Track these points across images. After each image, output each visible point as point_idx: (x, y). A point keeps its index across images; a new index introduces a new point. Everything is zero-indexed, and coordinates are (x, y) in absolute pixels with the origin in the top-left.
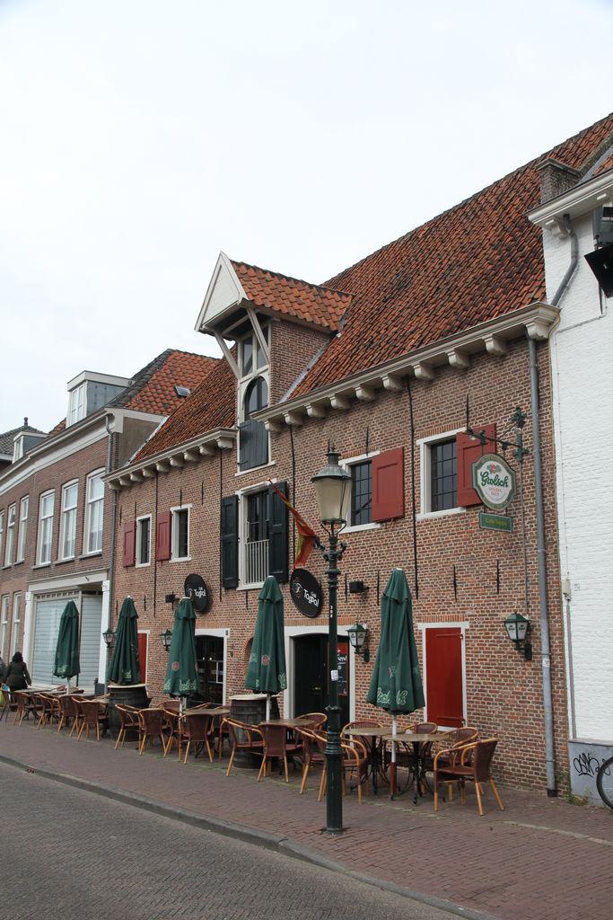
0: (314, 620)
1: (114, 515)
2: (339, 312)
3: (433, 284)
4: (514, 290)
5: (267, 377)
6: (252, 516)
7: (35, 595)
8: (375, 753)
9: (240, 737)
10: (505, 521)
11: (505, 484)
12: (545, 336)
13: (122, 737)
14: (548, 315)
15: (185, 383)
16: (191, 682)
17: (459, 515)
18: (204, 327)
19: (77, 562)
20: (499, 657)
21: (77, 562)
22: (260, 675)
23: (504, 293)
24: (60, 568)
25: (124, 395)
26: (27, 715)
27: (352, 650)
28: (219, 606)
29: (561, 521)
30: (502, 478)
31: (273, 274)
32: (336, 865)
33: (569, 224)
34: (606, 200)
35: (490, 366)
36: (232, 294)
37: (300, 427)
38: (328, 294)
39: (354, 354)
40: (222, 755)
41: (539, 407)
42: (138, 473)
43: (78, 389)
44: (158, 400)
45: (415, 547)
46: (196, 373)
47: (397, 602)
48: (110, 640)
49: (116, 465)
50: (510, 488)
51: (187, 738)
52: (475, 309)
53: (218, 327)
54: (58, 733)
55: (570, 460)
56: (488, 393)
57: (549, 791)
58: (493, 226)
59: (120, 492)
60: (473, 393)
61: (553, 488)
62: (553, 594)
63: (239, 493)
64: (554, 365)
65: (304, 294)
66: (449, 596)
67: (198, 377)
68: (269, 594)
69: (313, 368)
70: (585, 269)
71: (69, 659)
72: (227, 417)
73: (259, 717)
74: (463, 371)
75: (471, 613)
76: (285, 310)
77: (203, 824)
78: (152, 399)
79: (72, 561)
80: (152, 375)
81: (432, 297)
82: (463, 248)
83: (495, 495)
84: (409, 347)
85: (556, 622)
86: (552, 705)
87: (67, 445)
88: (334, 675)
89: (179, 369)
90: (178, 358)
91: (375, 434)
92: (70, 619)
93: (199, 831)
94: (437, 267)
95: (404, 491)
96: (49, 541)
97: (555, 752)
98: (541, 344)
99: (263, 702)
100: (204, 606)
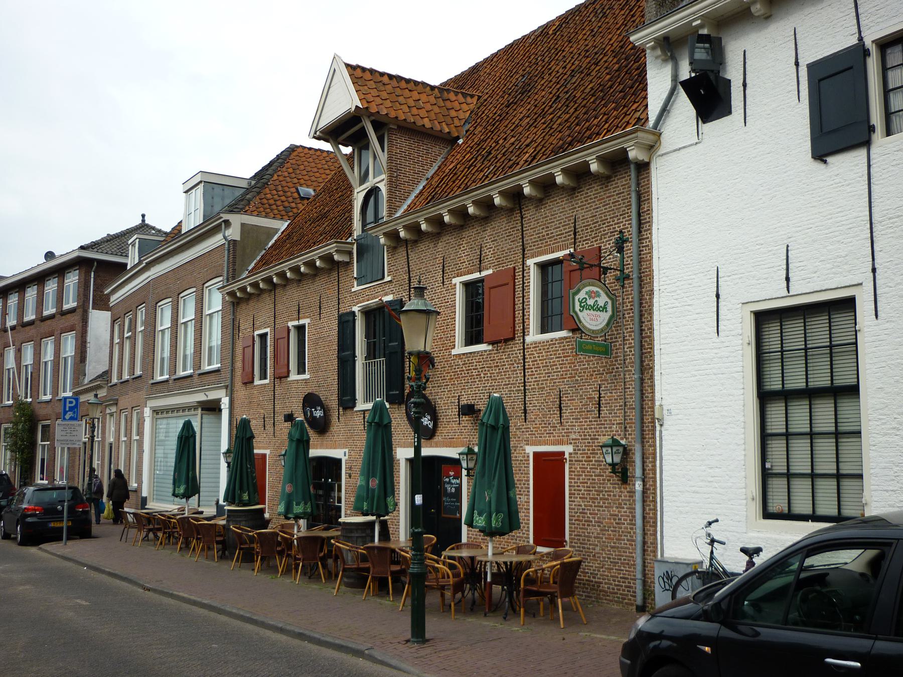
0: (429, 441)
1: (232, 328)
2: (462, 115)
3: (554, 92)
4: (624, 106)
5: (383, 187)
6: (370, 333)
7: (154, 411)
8: (472, 571)
9: (350, 558)
10: (601, 347)
11: (604, 309)
12: (646, 160)
13: (238, 558)
14: (647, 138)
15: (309, 183)
16: (306, 504)
17: (566, 338)
18: (318, 133)
19: (196, 377)
20: (599, 480)
21: (196, 377)
22: (368, 497)
23: (615, 109)
24: (178, 384)
25: (242, 199)
26: (147, 536)
27: (464, 472)
28: (338, 426)
29: (656, 347)
30: (601, 303)
31: (391, 77)
32: (412, 669)
33: (669, 46)
34: (701, 26)
35: (596, 187)
36: (346, 100)
37: (415, 242)
38: (452, 96)
39: (471, 165)
40: (331, 576)
41: (640, 232)
42: (255, 285)
43: (193, 191)
44: (279, 203)
45: (524, 370)
46: (321, 171)
47: (494, 428)
48: (230, 460)
49: (233, 276)
50: (610, 313)
51: (299, 559)
52: (587, 124)
53: (334, 132)
54: (176, 554)
55: (666, 287)
56: (597, 212)
57: (637, 607)
58: (618, 29)
59: (238, 303)
60: (580, 214)
61: (651, 313)
62: (648, 419)
63: (356, 309)
64: (654, 189)
65: (424, 98)
66: (555, 420)
67: (324, 176)
68: (377, 418)
69: (432, 177)
70: (683, 98)
71: (187, 480)
72: (343, 229)
73: (368, 539)
74: (571, 191)
75: (574, 437)
76: (402, 117)
77: (301, 636)
78: (272, 202)
79: (190, 376)
80: (272, 176)
81: (551, 107)
82: (587, 51)
83: (593, 321)
84: (522, 163)
85: (650, 446)
86: (644, 526)
87: (183, 251)
88: (419, 499)
89: (302, 167)
90: (302, 155)
91: (488, 253)
92: (187, 438)
93: (296, 642)
94: (561, 71)
95: (514, 312)
96: (167, 354)
97: (644, 570)
98: (643, 167)
99: (371, 524)
100: (322, 427)
